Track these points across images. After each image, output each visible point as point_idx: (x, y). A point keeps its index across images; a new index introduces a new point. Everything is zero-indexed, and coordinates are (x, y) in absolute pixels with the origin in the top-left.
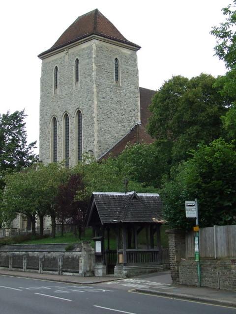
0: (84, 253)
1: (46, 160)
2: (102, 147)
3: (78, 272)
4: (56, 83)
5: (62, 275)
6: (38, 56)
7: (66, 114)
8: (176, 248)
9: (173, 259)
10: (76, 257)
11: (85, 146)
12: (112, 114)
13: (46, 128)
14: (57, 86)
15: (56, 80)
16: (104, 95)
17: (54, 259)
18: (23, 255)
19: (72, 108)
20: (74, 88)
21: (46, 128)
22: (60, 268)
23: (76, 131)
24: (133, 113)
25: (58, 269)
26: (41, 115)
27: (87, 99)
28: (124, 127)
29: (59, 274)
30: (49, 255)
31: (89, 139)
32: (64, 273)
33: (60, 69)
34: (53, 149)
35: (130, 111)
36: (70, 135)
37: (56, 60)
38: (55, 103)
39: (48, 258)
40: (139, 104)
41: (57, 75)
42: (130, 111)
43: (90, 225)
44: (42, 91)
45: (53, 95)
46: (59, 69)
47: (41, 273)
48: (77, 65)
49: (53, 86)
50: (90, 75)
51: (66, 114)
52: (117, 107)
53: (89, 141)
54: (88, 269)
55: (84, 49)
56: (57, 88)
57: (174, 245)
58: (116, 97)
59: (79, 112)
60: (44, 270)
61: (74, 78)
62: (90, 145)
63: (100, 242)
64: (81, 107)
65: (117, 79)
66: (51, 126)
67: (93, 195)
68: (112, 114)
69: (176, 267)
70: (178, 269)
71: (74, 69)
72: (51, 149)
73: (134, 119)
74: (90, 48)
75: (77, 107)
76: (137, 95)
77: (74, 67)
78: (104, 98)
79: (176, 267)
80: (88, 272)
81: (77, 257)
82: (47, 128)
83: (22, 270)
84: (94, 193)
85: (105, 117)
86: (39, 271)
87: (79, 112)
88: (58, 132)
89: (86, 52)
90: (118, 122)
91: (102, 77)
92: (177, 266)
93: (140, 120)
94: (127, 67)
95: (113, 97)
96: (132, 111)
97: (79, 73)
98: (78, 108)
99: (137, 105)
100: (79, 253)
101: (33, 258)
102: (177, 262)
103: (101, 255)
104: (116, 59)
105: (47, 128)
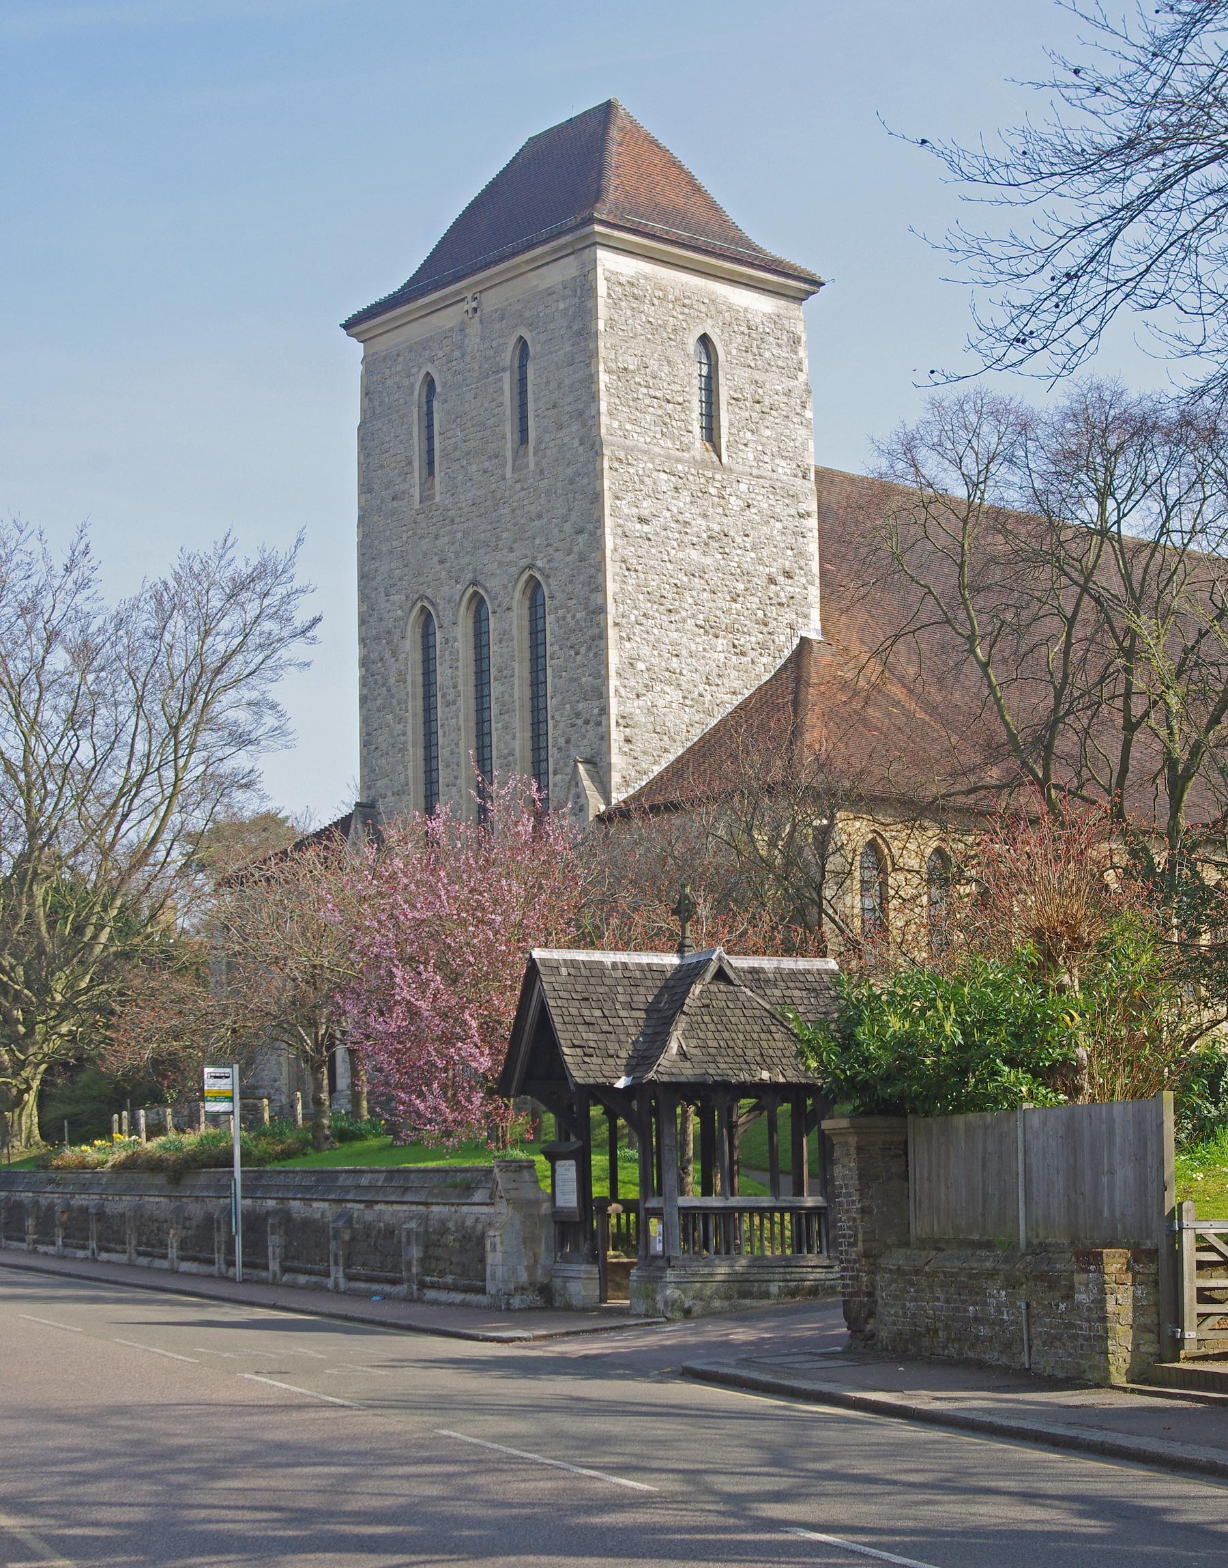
0: (503, 1211)
1: (390, 799)
2: (638, 746)
3: (482, 1291)
4: (430, 451)
5: (420, 1300)
6: (348, 326)
7: (476, 593)
8: (862, 1196)
9: (850, 1244)
10: (474, 1228)
11: (562, 741)
12: (687, 594)
13: (387, 656)
14: (431, 464)
15: (430, 438)
16: (647, 507)
17: (390, 1232)
18: (268, 1214)
19: (500, 563)
20: (509, 474)
21: (387, 656)
22: (409, 1269)
23: (521, 670)
24: (787, 588)
25: (404, 1274)
26: (363, 597)
27: (568, 527)
28: (743, 654)
29: (409, 1299)
30: (369, 1216)
31: (581, 706)
32: (431, 1294)
33: (444, 385)
34: (420, 753)
35: (772, 581)
36: (495, 688)
37: (425, 345)
38: (424, 545)
39: (368, 1227)
40: (813, 547)
41: (430, 414)
42: (772, 581)
43: (522, 1091)
44: (366, 486)
45: (417, 506)
46: (438, 390)
47: (336, 1290)
48: (523, 367)
49: (416, 464)
50: (581, 414)
51: (476, 593)
52: (708, 561)
53: (578, 715)
54: (524, 1277)
55: (550, 292)
56: (431, 473)
57: (855, 1182)
58: (705, 516)
59: (534, 588)
60: (350, 1278)
61: (509, 429)
62: (584, 737)
63: (573, 1162)
64: (539, 563)
65: (711, 432)
66: (410, 647)
67: (532, 964)
68: (687, 594)
69: (865, 1278)
70: (873, 1284)
71: (507, 386)
72: (415, 754)
73: (789, 616)
74: (630, 290)
75: (524, 562)
76: (803, 507)
77: (506, 377)
78: (642, 520)
79: (865, 1278)
80: (521, 1289)
81: (480, 1226)
82: (394, 654)
83: (264, 1274)
84: (537, 953)
85: (652, 609)
86: (330, 1283)
87: (534, 588)
88: (442, 674)
89: (561, 306)
90: (710, 628)
91: (635, 422)
92: (868, 1273)
93: (815, 614)
94: (757, 376)
95: (687, 516)
96: (781, 579)
97: (531, 406)
98: (531, 567)
99: (801, 554)
100: (484, 1209)
101: (308, 1226)
102: (866, 1254)
103: (578, 1219)
104: (704, 340)
105: (394, 654)
